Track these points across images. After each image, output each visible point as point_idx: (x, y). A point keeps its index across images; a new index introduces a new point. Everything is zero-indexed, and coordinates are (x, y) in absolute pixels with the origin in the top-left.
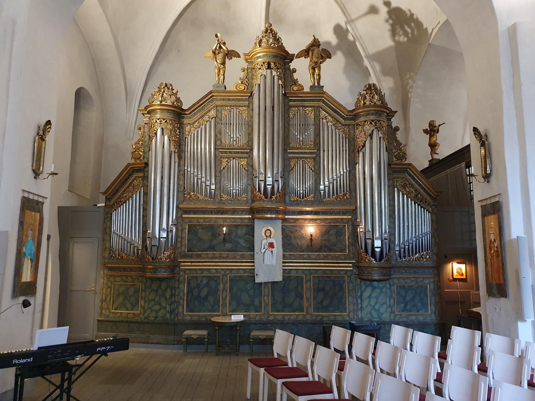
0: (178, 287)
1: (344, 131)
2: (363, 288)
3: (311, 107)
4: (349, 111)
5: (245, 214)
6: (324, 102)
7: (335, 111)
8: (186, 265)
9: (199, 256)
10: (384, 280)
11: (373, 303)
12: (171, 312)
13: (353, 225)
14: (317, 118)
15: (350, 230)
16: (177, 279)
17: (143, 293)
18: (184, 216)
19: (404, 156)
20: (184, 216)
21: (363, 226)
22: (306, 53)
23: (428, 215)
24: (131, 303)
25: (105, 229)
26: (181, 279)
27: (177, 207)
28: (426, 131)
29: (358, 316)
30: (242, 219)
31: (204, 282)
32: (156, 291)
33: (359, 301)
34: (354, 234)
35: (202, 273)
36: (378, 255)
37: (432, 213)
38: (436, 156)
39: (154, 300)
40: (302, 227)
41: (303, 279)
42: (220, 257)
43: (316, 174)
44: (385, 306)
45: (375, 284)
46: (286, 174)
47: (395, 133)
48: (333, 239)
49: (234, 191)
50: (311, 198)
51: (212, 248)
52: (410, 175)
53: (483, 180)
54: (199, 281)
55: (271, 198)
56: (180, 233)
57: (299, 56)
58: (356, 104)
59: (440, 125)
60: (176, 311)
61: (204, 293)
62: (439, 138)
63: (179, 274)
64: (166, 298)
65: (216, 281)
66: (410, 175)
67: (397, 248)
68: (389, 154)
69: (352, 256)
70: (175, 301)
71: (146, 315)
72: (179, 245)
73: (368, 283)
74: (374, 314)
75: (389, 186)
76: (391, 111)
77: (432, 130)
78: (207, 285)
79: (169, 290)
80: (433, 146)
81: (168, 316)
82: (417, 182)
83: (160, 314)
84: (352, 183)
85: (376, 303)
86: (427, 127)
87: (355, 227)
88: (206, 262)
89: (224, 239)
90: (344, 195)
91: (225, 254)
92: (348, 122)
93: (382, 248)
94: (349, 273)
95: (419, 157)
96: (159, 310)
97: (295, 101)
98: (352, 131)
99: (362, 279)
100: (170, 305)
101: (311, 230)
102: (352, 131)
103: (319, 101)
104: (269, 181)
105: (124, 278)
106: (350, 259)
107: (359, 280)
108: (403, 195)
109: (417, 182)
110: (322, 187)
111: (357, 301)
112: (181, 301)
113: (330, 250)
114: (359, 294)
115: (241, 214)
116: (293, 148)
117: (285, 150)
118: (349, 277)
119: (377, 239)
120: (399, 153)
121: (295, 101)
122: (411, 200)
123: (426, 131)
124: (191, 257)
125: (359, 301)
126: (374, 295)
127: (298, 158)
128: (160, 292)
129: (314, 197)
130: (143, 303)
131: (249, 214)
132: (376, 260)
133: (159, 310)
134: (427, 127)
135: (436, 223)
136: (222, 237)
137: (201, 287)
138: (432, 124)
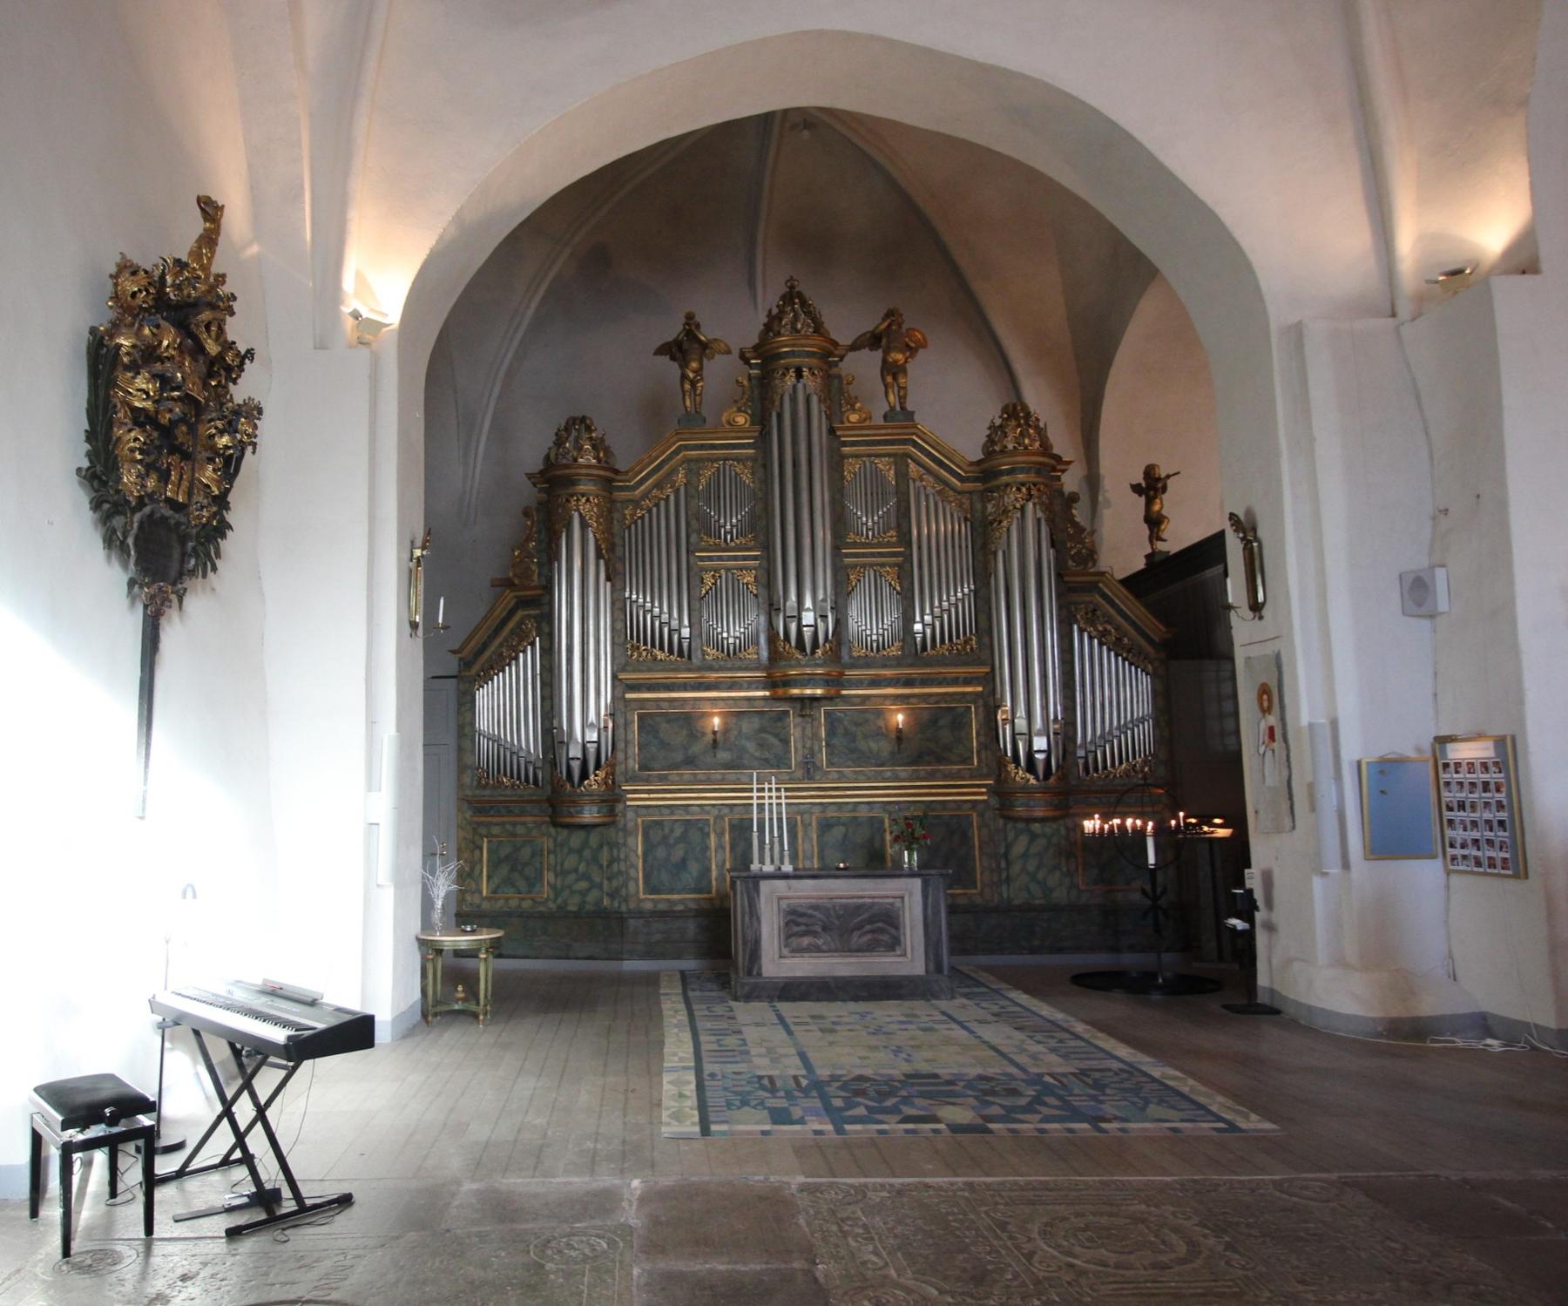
0: (625, 844)
1: (960, 505)
2: (1011, 836)
3: (889, 455)
4: (971, 464)
5: (757, 689)
6: (915, 445)
7: (941, 464)
8: (638, 798)
9: (663, 779)
10: (1054, 819)
11: (1031, 867)
12: (612, 896)
13: (986, 705)
14: (902, 475)
15: (981, 716)
16: (621, 825)
17: (552, 857)
18: (628, 696)
19: (1091, 555)
20: (628, 696)
21: (1008, 708)
22: (873, 340)
23: (1145, 682)
24: (527, 879)
25: (461, 727)
26: (630, 825)
27: (614, 677)
28: (1136, 489)
29: (1001, 894)
30: (749, 699)
31: (678, 832)
32: (580, 852)
33: (1003, 864)
34: (991, 728)
35: (672, 814)
36: (1040, 769)
37: (1154, 676)
38: (1160, 546)
39: (576, 870)
40: (879, 713)
41: (882, 822)
42: (709, 781)
43: (904, 598)
44: (1057, 874)
45: (1036, 827)
46: (840, 601)
47: (1070, 508)
48: (946, 735)
49: (731, 640)
50: (894, 651)
51: (690, 762)
52: (1104, 596)
53: (1250, 614)
54: (667, 830)
55: (813, 652)
56: (621, 730)
57: (855, 347)
58: (985, 447)
59: (1168, 477)
60: (623, 892)
61: (679, 853)
62: (1167, 504)
63: (624, 816)
64: (601, 867)
65: (701, 829)
66: (1104, 596)
67: (1081, 753)
68: (1057, 551)
69: (985, 771)
70: (620, 872)
71: (559, 901)
72: (620, 756)
73: (1021, 825)
74: (1033, 887)
75: (1060, 622)
76: (1058, 458)
77: (1152, 486)
78: (683, 838)
79: (605, 848)
80: (1154, 522)
81: (606, 902)
82: (1120, 611)
83: (592, 897)
84: (982, 617)
85: (1038, 868)
86: (1139, 479)
87: (990, 705)
88: (680, 791)
89: (715, 741)
90: (966, 642)
91: (717, 774)
92: (969, 486)
93: (1048, 752)
94: (980, 807)
95: (1122, 548)
96: (589, 889)
97: (853, 444)
98: (978, 506)
99: (1008, 818)
100: (609, 879)
101: (900, 718)
102: (978, 506)
103: (905, 442)
104: (808, 618)
105: (509, 827)
106: (986, 777)
107: (1001, 822)
108: (1091, 638)
109: (1120, 611)
110: (918, 627)
111: (999, 864)
112: (632, 872)
113: (940, 760)
114: (1002, 851)
115: (748, 689)
116: (855, 545)
117: (836, 548)
118: (981, 815)
119: (1039, 734)
120: (1079, 552)
121: (853, 444)
122: (1109, 650)
123: (1136, 489)
124: (648, 781)
125: (1003, 864)
126: (1033, 850)
127: (864, 566)
128: (587, 853)
129: (902, 648)
130: (552, 876)
131: (764, 689)
132: (1037, 778)
133: (589, 889)
134: (1139, 479)
135: (1164, 700)
136: (710, 737)
137: (672, 841)
138: (1149, 472)
